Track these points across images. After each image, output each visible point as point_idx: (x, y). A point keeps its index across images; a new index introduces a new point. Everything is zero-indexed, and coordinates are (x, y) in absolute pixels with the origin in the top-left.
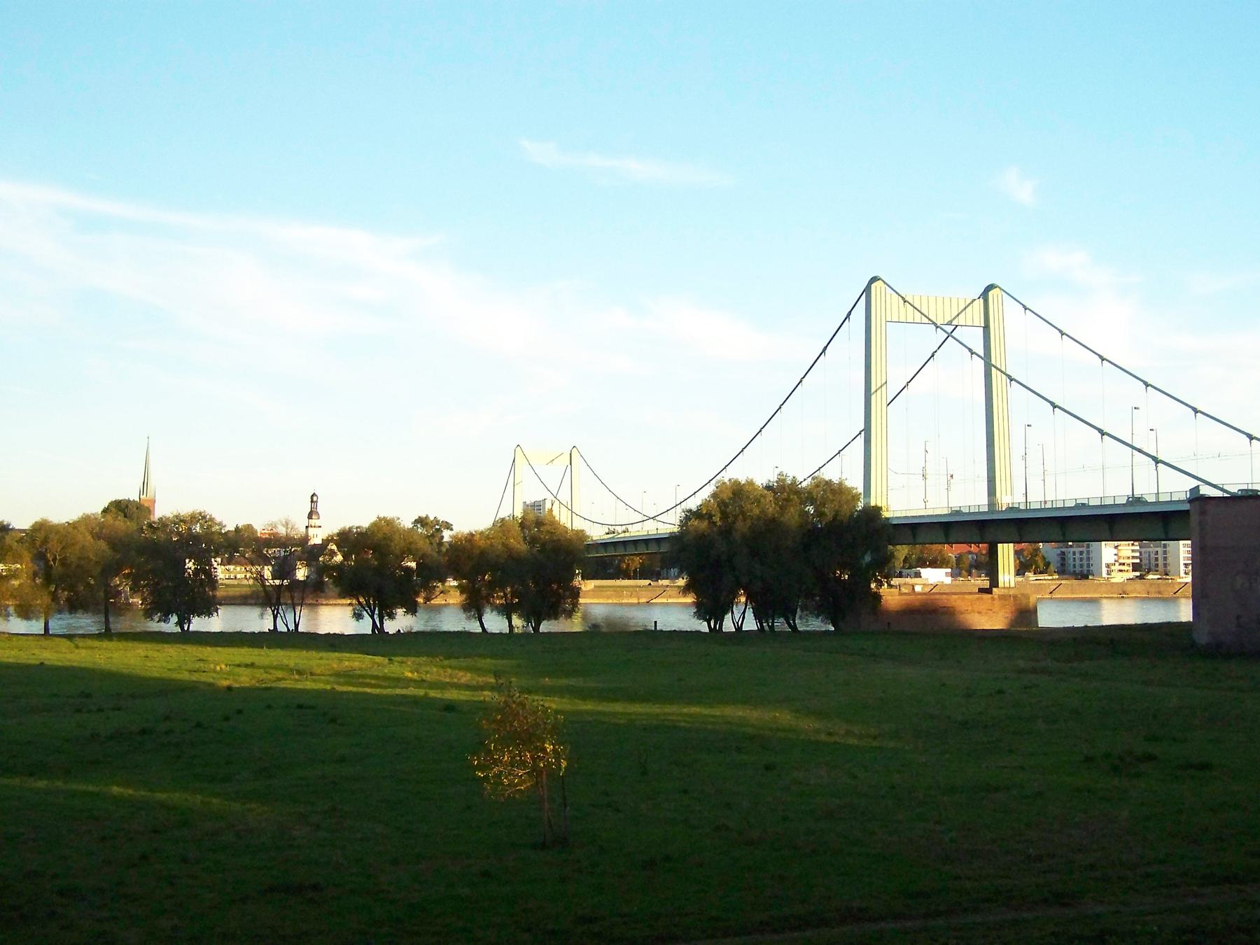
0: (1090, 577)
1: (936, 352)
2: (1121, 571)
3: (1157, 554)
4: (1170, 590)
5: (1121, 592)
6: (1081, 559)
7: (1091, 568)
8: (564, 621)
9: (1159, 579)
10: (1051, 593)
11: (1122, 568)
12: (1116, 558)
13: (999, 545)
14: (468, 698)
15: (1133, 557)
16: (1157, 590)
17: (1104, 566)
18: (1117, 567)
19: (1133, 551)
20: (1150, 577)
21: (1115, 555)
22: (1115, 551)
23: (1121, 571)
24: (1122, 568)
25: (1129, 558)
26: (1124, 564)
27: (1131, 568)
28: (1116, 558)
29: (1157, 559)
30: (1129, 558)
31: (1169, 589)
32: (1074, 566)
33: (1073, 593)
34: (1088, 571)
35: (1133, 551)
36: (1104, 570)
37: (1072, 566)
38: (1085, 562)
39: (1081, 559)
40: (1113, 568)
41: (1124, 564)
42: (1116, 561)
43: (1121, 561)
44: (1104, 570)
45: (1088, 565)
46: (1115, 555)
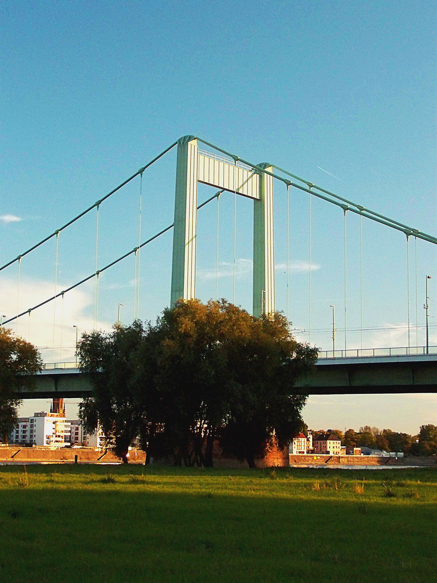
0: (34, 446)
1: (138, 248)
2: (57, 441)
3: (78, 430)
4: (95, 457)
5: (62, 458)
6: (24, 432)
7: (34, 439)
8: (35, 346)
9: (80, 448)
10: (12, 457)
11: (58, 439)
12: (54, 431)
13: (52, 399)
14: (41, 486)
15: (66, 432)
16: (86, 456)
17: (45, 437)
18: (54, 439)
19: (66, 426)
20: (76, 447)
21: (54, 429)
22: (54, 426)
23: (57, 441)
24: (58, 439)
25: (62, 431)
26: (59, 436)
27: (63, 440)
28: (54, 431)
29: (77, 434)
30: (62, 431)
31: (94, 456)
32: (17, 437)
33: (28, 458)
34: (31, 441)
35: (66, 426)
36: (45, 440)
37: (14, 436)
38: (28, 434)
39: (24, 432)
40: (52, 439)
41: (59, 436)
42: (53, 434)
43: (58, 434)
44: (45, 440)
45: (31, 436)
46: (54, 429)
